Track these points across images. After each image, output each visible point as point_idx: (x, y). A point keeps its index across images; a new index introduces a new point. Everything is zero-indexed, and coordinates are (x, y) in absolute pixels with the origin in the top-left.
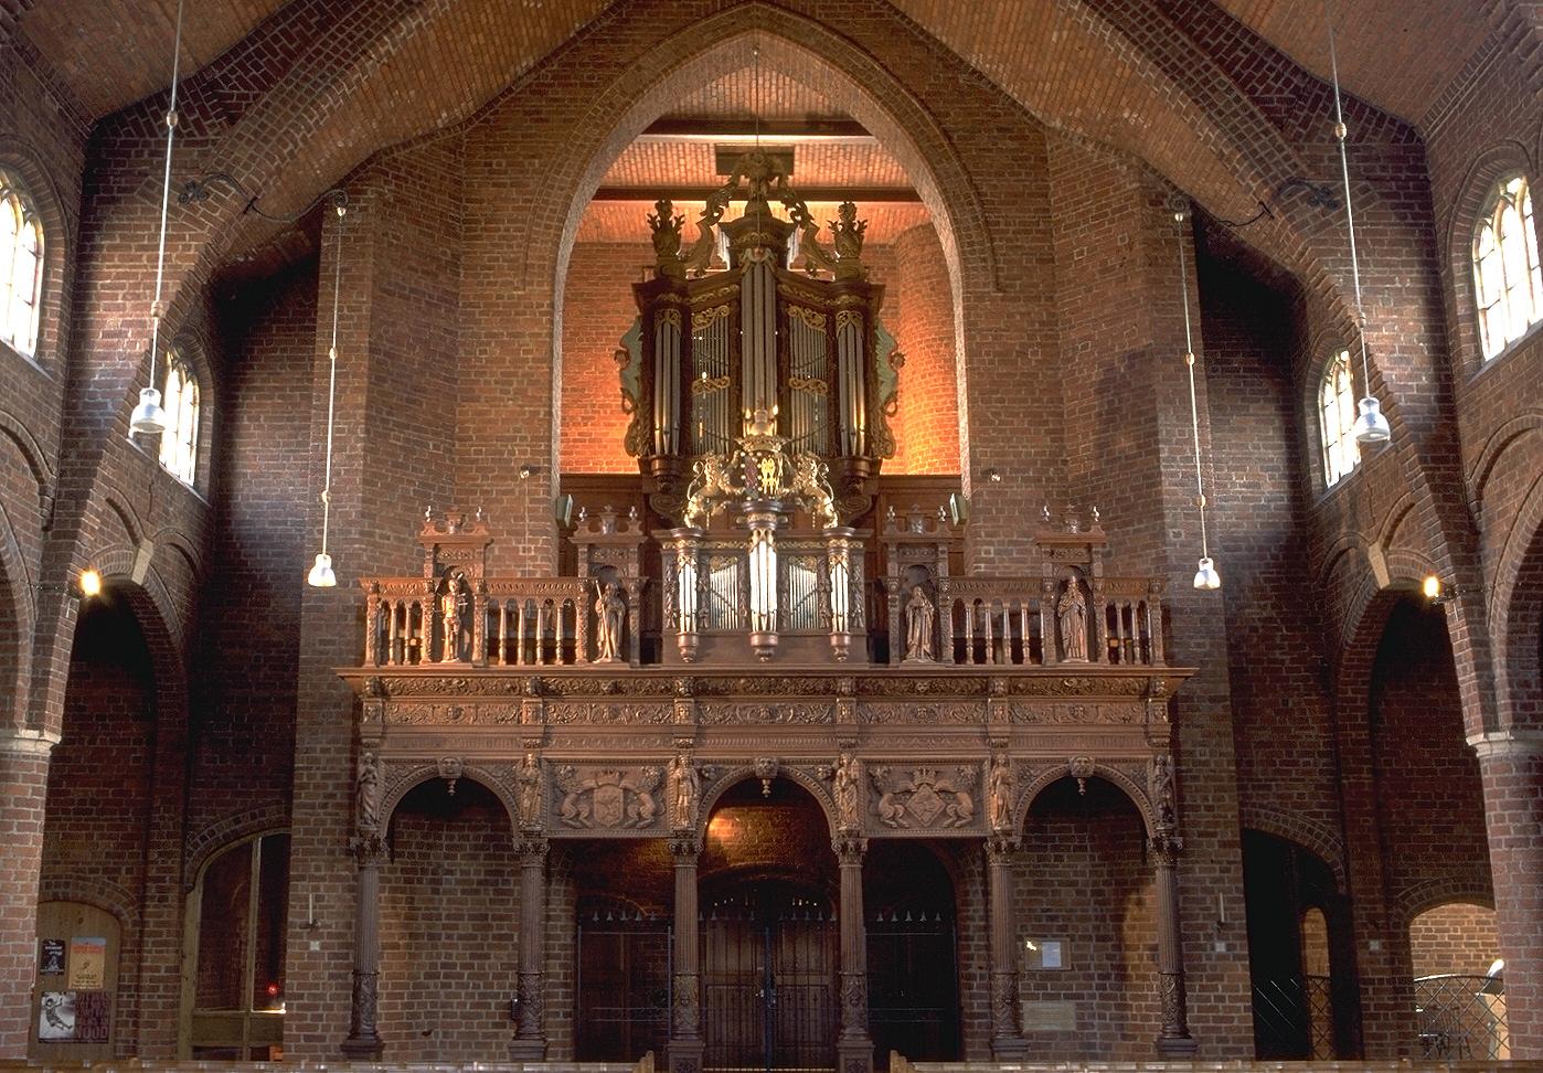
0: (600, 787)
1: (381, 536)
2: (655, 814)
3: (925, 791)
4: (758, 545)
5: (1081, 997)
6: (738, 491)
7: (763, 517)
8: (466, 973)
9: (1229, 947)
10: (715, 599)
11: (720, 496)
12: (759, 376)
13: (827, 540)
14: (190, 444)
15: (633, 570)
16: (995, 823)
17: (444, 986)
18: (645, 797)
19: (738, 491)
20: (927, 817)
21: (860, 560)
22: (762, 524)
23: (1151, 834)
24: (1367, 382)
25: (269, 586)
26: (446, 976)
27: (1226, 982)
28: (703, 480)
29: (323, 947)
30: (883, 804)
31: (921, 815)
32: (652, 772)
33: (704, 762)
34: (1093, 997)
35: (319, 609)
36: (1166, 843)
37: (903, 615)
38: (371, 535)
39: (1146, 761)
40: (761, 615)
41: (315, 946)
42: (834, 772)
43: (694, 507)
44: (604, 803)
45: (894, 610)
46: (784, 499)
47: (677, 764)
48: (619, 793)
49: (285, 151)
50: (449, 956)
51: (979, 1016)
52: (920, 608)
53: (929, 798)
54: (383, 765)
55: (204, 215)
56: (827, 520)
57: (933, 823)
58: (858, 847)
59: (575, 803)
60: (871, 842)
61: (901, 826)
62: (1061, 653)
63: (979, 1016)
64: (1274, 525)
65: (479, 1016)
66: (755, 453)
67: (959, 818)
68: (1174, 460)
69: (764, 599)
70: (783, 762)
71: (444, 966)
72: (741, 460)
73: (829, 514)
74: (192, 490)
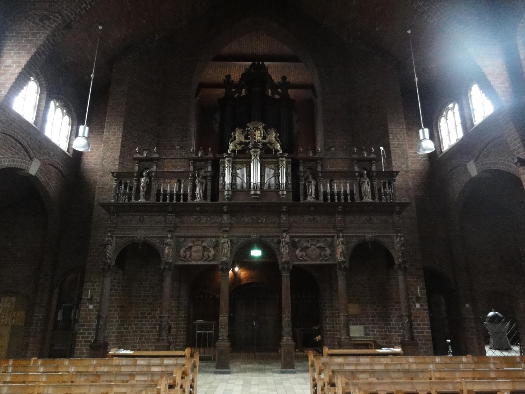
0: (194, 246)
1: (126, 164)
2: (214, 255)
3: (314, 247)
4: (254, 160)
5: (365, 324)
6: (247, 141)
7: (256, 150)
8: (149, 316)
9: (421, 306)
10: (238, 179)
11: (241, 143)
12: (256, 165)
13: (278, 158)
14: (67, 137)
15: (209, 169)
16: (340, 258)
17: (141, 321)
18: (211, 249)
19: (247, 141)
20: (314, 256)
21: (290, 165)
22: (255, 152)
23: (397, 263)
24: (486, 87)
25: (92, 185)
26: (141, 318)
27: (420, 319)
28: (235, 138)
29: (94, 307)
30: (298, 252)
31: (311, 255)
32: (214, 240)
33: (232, 237)
34: (370, 324)
35: (103, 188)
36: (403, 266)
37: (305, 185)
38: (123, 163)
39: (393, 236)
40: (254, 184)
41: (91, 307)
42: (280, 240)
43: (231, 146)
44: (196, 252)
45: (302, 183)
46: (264, 144)
47: (223, 237)
48: (201, 248)
49: (82, 7)
50: (143, 310)
51: (329, 331)
52: (311, 182)
53: (315, 249)
54: (115, 239)
55: (48, 26)
56: (278, 151)
57: (316, 259)
58: (288, 268)
59: (185, 251)
60: (293, 266)
61: (305, 260)
62: (361, 198)
63: (329, 331)
64: (423, 165)
65: (153, 332)
66: (253, 128)
67: (326, 257)
68: (394, 139)
69: (255, 178)
70: (261, 237)
71: (141, 314)
72: (248, 131)
73: (279, 149)
74: (34, 125)
